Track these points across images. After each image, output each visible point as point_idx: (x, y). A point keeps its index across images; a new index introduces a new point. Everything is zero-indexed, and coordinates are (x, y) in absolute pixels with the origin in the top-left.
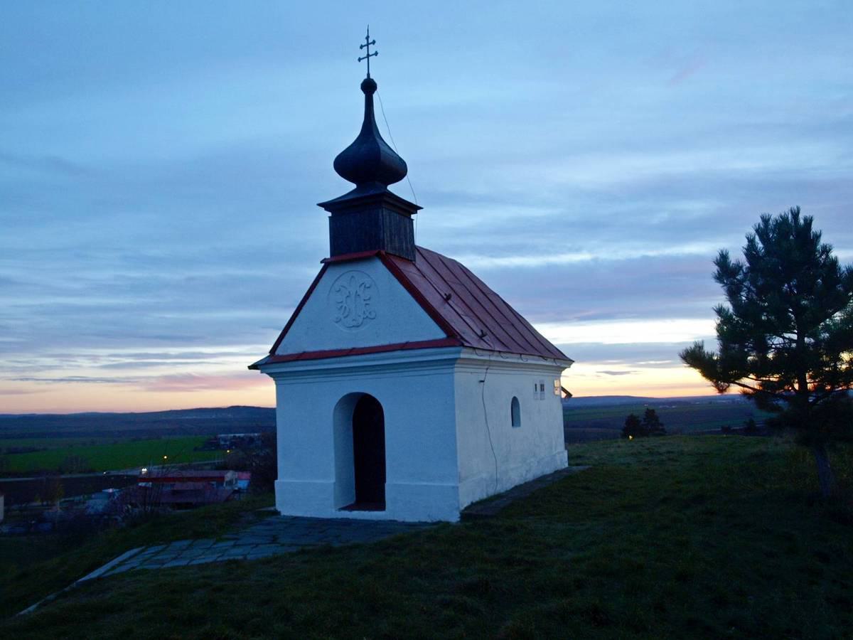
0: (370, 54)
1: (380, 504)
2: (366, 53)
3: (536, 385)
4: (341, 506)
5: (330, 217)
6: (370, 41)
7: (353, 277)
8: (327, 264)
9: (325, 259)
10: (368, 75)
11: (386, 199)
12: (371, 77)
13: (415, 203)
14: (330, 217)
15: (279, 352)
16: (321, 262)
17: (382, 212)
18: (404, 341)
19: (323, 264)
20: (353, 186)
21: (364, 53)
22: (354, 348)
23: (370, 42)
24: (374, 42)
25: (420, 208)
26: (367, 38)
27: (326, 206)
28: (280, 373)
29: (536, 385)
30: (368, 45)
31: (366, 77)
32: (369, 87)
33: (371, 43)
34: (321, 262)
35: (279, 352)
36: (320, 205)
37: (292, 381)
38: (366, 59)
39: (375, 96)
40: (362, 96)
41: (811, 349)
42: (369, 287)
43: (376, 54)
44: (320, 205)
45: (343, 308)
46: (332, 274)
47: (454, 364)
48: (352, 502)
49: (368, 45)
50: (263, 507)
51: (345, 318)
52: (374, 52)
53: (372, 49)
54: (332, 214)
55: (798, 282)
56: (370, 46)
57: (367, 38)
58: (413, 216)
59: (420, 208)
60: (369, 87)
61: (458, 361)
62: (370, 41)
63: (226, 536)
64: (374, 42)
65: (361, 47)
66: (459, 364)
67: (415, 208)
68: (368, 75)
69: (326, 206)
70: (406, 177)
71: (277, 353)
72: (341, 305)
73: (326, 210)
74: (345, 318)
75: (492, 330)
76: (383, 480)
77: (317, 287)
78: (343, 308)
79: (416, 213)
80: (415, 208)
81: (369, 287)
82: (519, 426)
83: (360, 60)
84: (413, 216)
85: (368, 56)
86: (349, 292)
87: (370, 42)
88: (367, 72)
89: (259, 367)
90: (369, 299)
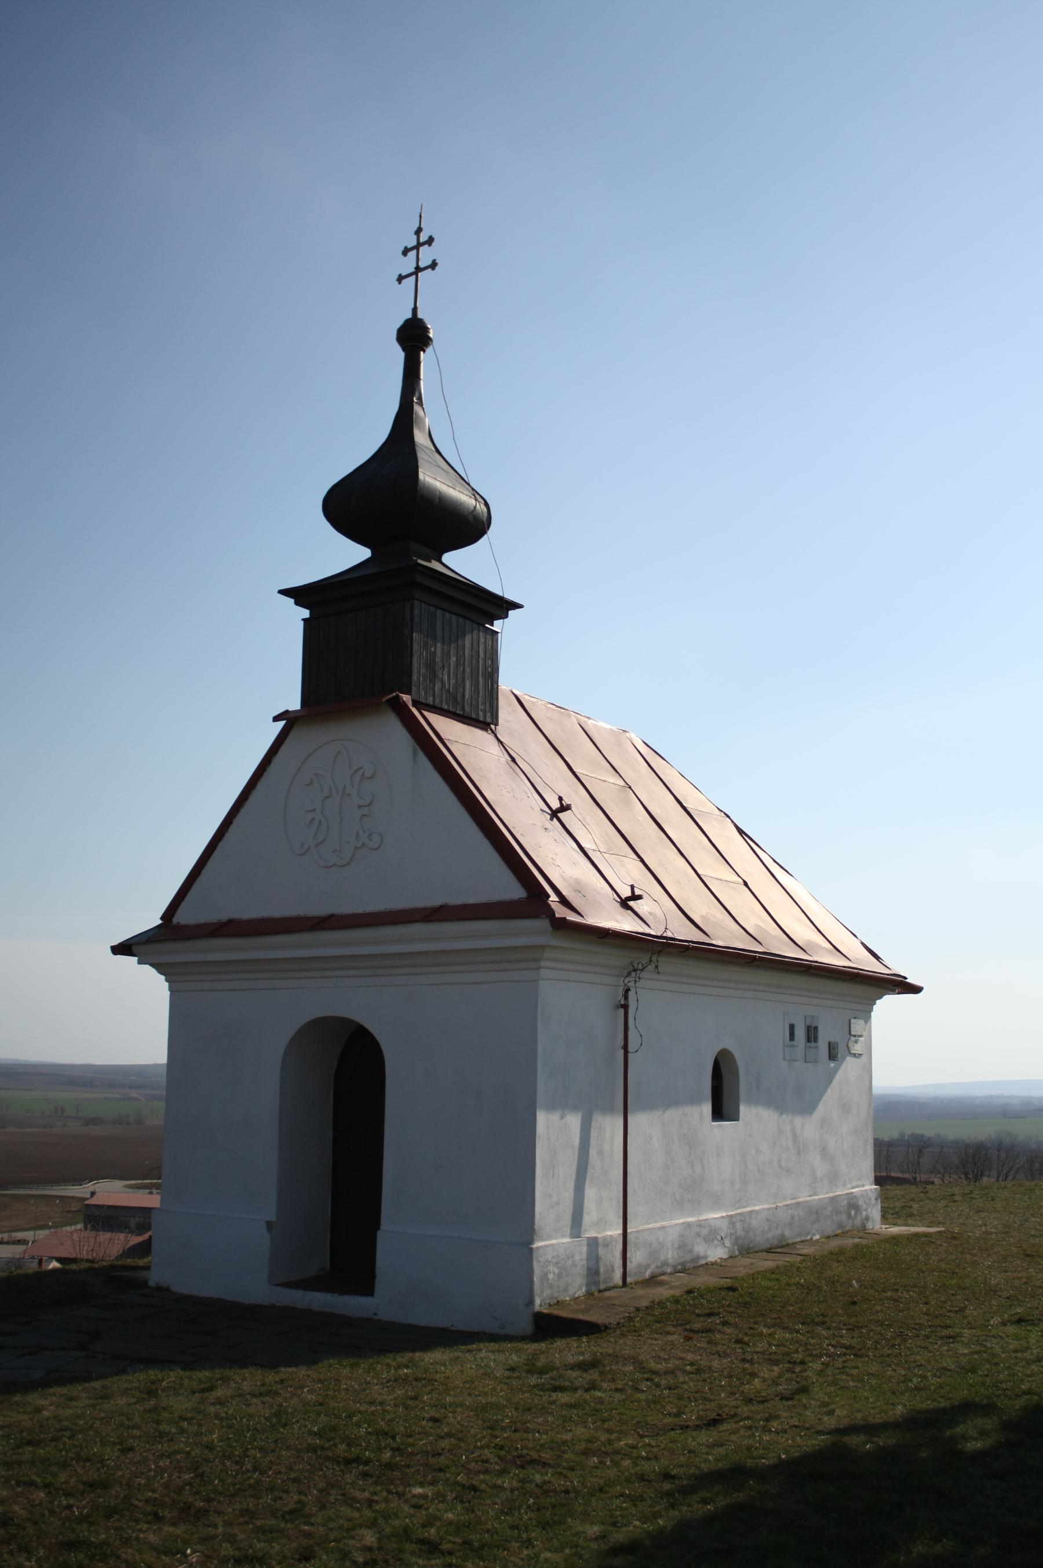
1: (368, 1289)
2: (415, 265)
3: (792, 1027)
6: (423, 238)
9: (287, 712)
10: (415, 310)
11: (420, 579)
12: (420, 315)
15: (179, 918)
16: (276, 719)
17: (412, 609)
19: (281, 724)
20: (363, 553)
21: (408, 264)
22: (332, 916)
23: (422, 240)
24: (430, 241)
25: (516, 606)
27: (298, 595)
28: (229, 962)
29: (792, 1027)
31: (409, 315)
33: (412, 249)
34: (276, 719)
40: (399, 356)
42: (371, 777)
43: (433, 265)
44: (284, 592)
45: (316, 823)
46: (302, 740)
47: (539, 960)
52: (429, 263)
53: (426, 255)
54: (311, 614)
58: (306, 613)
59: (516, 606)
61: (547, 954)
63: (729, 1280)
67: (502, 606)
68: (415, 310)
69: (298, 595)
70: (485, 537)
71: (175, 921)
73: (297, 603)
75: (732, 885)
76: (377, 1226)
77: (265, 774)
78: (316, 823)
79: (507, 616)
80: (502, 606)
81: (371, 777)
82: (737, 1119)
83: (400, 279)
84: (497, 625)
85: (418, 269)
87: (422, 240)
89: (134, 949)
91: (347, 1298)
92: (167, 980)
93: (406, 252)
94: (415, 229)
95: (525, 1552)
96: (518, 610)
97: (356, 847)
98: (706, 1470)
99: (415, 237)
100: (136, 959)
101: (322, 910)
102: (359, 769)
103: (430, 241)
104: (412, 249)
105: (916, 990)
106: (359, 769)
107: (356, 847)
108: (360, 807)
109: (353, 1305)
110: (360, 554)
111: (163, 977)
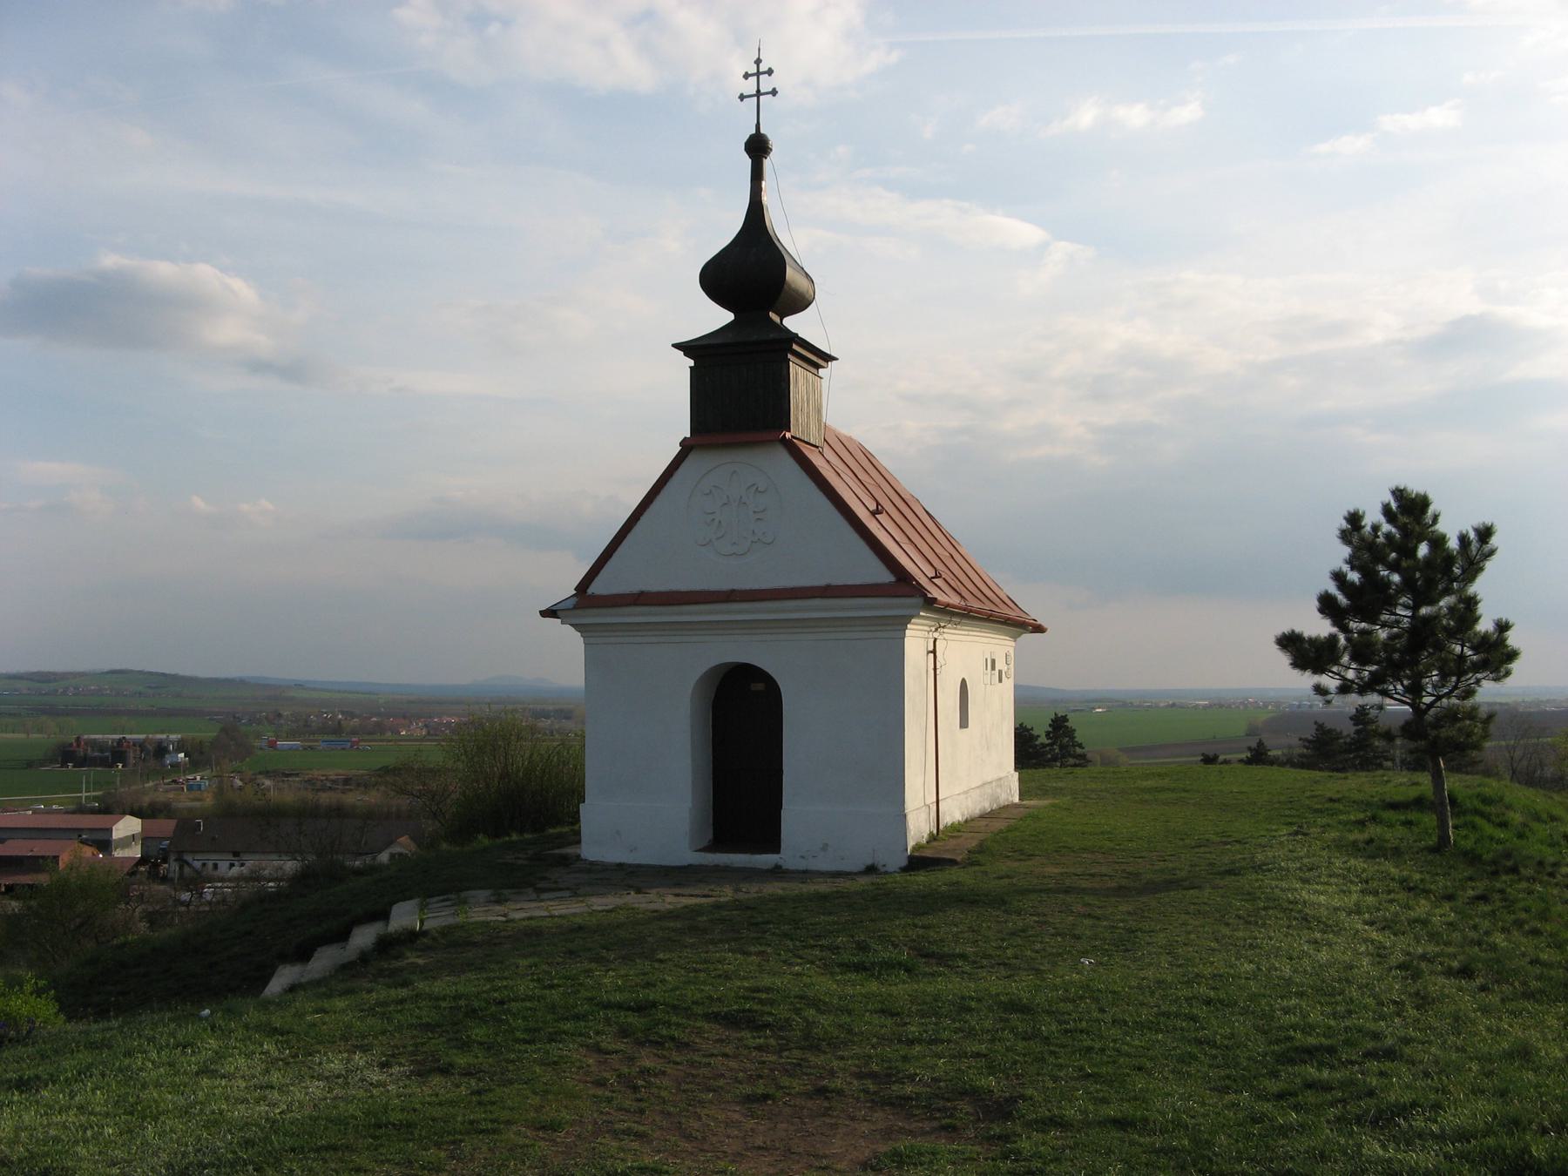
0: (762, 91)
1: (770, 839)
2: (756, 89)
3: (986, 660)
4: (699, 848)
5: (691, 367)
6: (763, 68)
7: (735, 472)
8: (687, 447)
11: (795, 347)
13: (828, 352)
14: (691, 367)
15: (596, 588)
18: (822, 582)
20: (725, 317)
25: (835, 359)
26: (758, 62)
29: (986, 660)
30: (758, 74)
32: (757, 147)
33: (764, 73)
34: (1364, 513)
35: (596, 588)
36: (677, 346)
37: (654, 639)
38: (756, 98)
39: (767, 163)
40: (746, 162)
41: (1307, 646)
44: (677, 346)
48: (705, 843)
49: (758, 74)
50: (552, 849)
51: (718, 539)
55: (1378, 564)
56: (761, 77)
57: (758, 62)
59: (835, 359)
60: (757, 147)
62: (763, 68)
64: (770, 72)
65: (746, 76)
66: (914, 624)
69: (686, 348)
71: (590, 591)
72: (711, 517)
73: (685, 355)
74: (718, 539)
83: (742, 97)
85: (758, 94)
86: (728, 497)
88: (756, 122)
89: (559, 613)
90: (764, 510)
91: (758, 857)
92: (582, 636)
93: (746, 76)
94: (755, 59)
95: (823, 1008)
96: (834, 362)
97: (752, 542)
98: (291, 873)
99: (755, 66)
100: (559, 620)
101: (725, 586)
102: (754, 485)
103: (770, 72)
104: (764, 73)
105: (1039, 629)
106: (754, 485)
107: (752, 542)
108: (755, 512)
109: (765, 860)
110: (725, 317)
111: (579, 634)
